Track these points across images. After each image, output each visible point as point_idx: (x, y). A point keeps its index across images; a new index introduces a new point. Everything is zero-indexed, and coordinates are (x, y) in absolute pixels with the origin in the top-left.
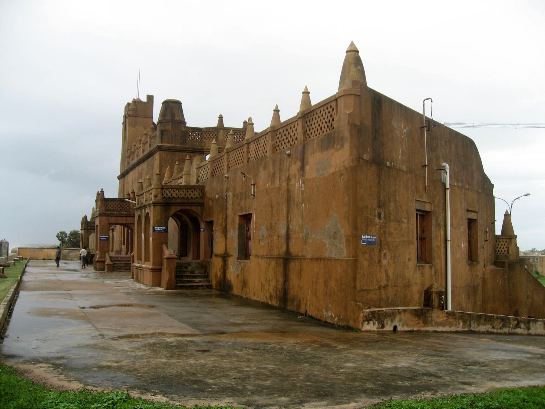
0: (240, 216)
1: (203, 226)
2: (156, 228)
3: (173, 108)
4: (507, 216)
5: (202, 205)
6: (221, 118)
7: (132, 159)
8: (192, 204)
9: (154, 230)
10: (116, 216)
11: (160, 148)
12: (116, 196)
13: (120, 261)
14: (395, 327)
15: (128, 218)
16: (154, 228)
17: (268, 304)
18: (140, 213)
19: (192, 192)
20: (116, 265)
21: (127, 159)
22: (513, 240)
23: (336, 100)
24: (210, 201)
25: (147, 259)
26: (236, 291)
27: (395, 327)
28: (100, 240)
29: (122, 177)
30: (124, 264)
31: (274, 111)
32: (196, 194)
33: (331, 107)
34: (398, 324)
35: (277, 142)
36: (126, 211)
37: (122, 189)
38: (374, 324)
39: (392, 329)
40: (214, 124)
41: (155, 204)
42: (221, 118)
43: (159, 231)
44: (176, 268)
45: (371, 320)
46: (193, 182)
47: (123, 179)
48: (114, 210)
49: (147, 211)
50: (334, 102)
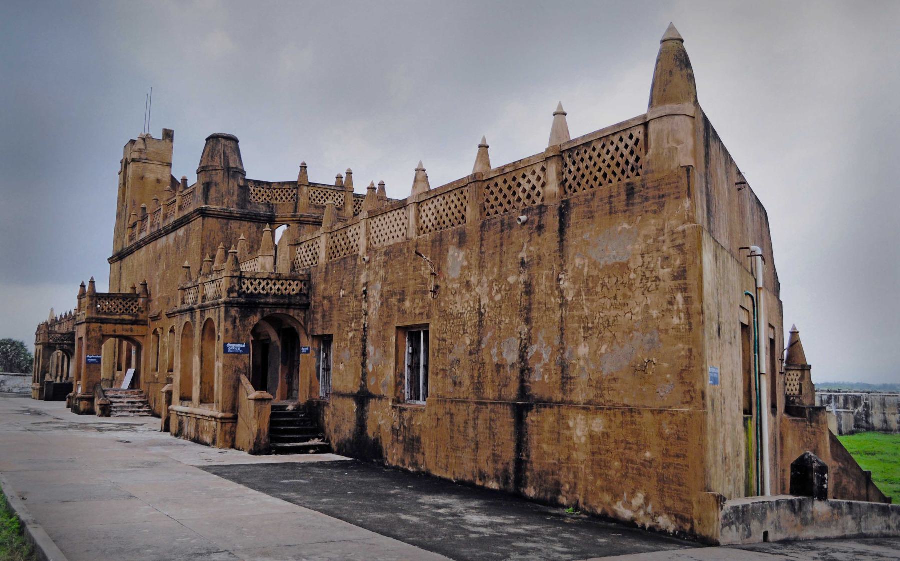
0: (397, 328)
1: (306, 343)
2: (229, 345)
3: (222, 149)
4: (794, 334)
5: (306, 307)
6: (304, 167)
7: (141, 232)
8: (289, 306)
9: (226, 350)
10: (116, 322)
11: (203, 213)
12: (107, 292)
13: (120, 398)
14: (766, 534)
15: (135, 327)
16: (225, 345)
17: (406, 471)
18: (189, 320)
19: (290, 285)
20: (115, 405)
21: (129, 231)
22: (806, 372)
23: (646, 125)
24: (326, 302)
25: (205, 400)
26: (394, 456)
27: (766, 534)
28: (87, 362)
29: (119, 257)
30: (128, 403)
31: (480, 147)
32: (295, 288)
33: (631, 137)
34: (769, 530)
35: (488, 201)
36: (133, 316)
37: (116, 278)
38: (738, 530)
39: (762, 538)
40: (294, 177)
41: (228, 305)
42: (304, 167)
43: (234, 352)
44: (272, 416)
45: (733, 523)
46: (284, 268)
47: (117, 264)
48: (111, 313)
49: (207, 317)
50: (641, 129)
